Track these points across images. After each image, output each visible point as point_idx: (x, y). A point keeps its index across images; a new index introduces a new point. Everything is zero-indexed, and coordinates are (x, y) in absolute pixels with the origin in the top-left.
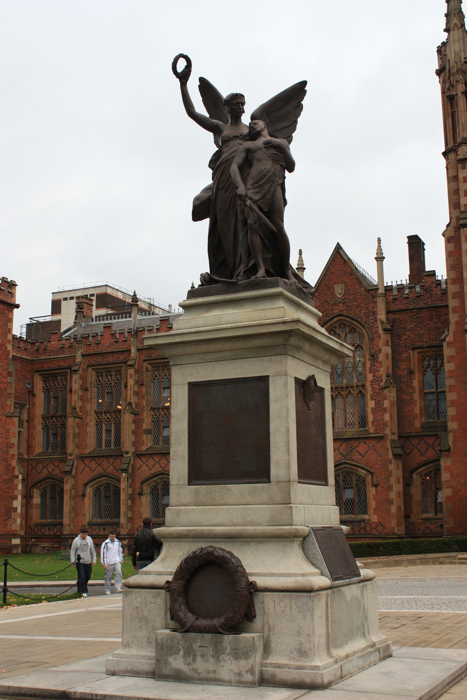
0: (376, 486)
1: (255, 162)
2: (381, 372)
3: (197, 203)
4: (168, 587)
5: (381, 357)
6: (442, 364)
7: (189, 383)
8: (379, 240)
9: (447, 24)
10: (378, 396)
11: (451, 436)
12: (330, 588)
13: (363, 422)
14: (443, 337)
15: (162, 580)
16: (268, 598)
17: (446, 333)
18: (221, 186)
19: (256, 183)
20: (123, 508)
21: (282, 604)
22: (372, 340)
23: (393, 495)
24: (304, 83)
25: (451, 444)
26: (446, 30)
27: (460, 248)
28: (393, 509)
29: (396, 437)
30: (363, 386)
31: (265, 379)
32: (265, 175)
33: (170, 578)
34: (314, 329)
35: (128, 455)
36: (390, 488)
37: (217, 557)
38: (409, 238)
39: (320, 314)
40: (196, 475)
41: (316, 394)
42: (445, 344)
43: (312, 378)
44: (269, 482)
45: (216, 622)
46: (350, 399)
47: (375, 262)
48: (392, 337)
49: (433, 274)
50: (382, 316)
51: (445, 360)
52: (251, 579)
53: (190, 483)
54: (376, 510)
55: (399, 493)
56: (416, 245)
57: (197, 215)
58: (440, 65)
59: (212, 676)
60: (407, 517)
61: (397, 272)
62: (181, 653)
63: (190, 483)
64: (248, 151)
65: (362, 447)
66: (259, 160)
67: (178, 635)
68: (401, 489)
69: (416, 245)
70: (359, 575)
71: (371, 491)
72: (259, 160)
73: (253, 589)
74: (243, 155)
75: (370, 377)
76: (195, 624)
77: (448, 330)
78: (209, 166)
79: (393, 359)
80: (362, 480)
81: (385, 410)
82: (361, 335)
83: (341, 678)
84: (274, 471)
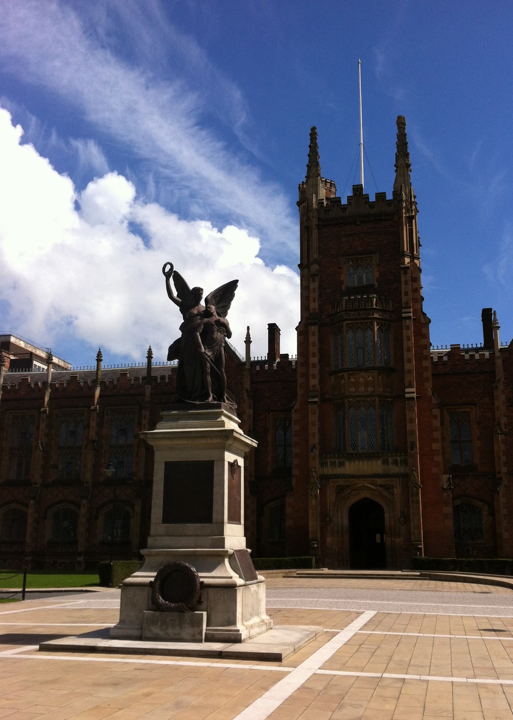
6: (290, 424)
8: (248, 328)
11: (294, 480)
12: (244, 585)
14: (292, 405)
17: (294, 402)
20: (29, 530)
21: (219, 595)
24: (237, 281)
25: (294, 485)
27: (308, 340)
29: (253, 479)
33: (153, 579)
34: (240, 434)
35: (37, 486)
38: (269, 325)
39: (240, 421)
40: (167, 519)
41: (237, 470)
42: (293, 411)
43: (236, 461)
49: (287, 356)
50: (247, 385)
51: (293, 422)
52: (201, 580)
56: (274, 331)
58: (300, 199)
59: (177, 636)
61: (260, 351)
62: (159, 624)
64: (206, 324)
67: (157, 613)
69: (274, 331)
70: (257, 579)
77: (296, 401)
78: (180, 329)
83: (249, 637)
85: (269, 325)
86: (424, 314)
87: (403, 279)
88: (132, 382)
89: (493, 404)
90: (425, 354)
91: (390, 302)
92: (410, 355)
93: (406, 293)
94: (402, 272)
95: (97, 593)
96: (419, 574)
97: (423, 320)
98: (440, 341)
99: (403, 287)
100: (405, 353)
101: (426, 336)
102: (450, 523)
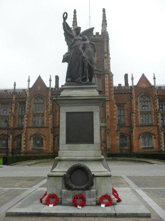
0: (46, 140)
1: (87, 48)
2: (49, 110)
3: (65, 57)
4: (64, 177)
5: (49, 106)
7: (66, 112)
9: (73, 24)
10: (48, 116)
13: (43, 123)
15: (62, 174)
16: (97, 179)
18: (75, 53)
19: (87, 54)
22: (47, 102)
23: (50, 142)
26: (72, 25)
28: (50, 146)
29: (52, 128)
30: (44, 114)
31: (92, 113)
32: (90, 52)
33: (65, 173)
36: (50, 141)
37: (82, 167)
38: (56, 76)
40: (68, 141)
44: (93, 144)
45: (83, 187)
46: (40, 117)
47: (131, 80)
48: (52, 101)
52: (93, 173)
53: (66, 144)
54: (46, 146)
55: (52, 142)
56: (57, 78)
57: (64, 61)
60: (54, 148)
63: (66, 144)
64: (84, 44)
65: (42, 130)
66: (88, 47)
67: (70, 191)
68: (53, 141)
69: (57, 78)
71: (44, 142)
72: (88, 47)
73: (94, 176)
74: (83, 45)
75: (46, 111)
76: (76, 188)
79: (52, 107)
80: (42, 139)
81: (49, 120)
82: (44, 100)
84: (95, 140)
85: (56, 76)
86: (111, 73)
87: (105, 61)
88: (9, 94)
89: (131, 104)
90: (112, 86)
91: (101, 68)
92: (107, 86)
93: (106, 66)
94: (105, 58)
95: (2, 168)
96: (112, 158)
97: (111, 75)
98: (116, 84)
99: (105, 64)
100: (106, 86)
101: (112, 80)
102: (118, 142)
